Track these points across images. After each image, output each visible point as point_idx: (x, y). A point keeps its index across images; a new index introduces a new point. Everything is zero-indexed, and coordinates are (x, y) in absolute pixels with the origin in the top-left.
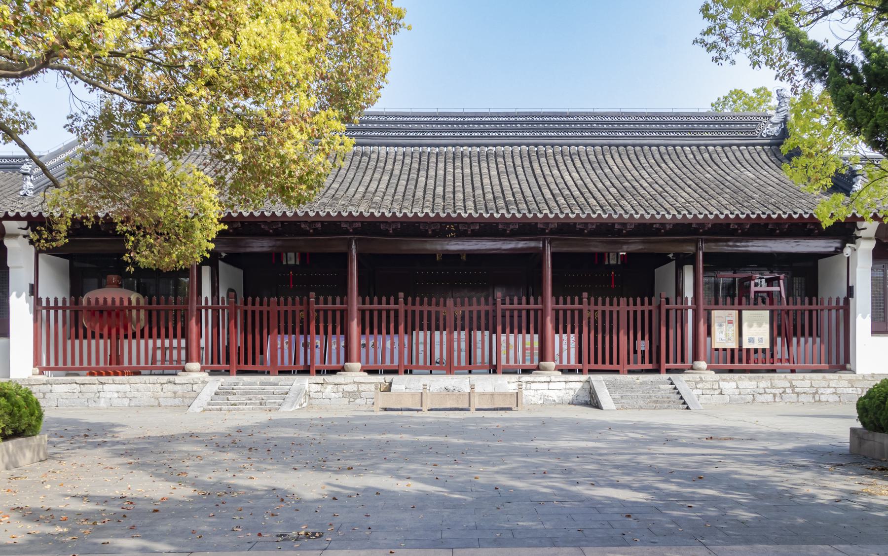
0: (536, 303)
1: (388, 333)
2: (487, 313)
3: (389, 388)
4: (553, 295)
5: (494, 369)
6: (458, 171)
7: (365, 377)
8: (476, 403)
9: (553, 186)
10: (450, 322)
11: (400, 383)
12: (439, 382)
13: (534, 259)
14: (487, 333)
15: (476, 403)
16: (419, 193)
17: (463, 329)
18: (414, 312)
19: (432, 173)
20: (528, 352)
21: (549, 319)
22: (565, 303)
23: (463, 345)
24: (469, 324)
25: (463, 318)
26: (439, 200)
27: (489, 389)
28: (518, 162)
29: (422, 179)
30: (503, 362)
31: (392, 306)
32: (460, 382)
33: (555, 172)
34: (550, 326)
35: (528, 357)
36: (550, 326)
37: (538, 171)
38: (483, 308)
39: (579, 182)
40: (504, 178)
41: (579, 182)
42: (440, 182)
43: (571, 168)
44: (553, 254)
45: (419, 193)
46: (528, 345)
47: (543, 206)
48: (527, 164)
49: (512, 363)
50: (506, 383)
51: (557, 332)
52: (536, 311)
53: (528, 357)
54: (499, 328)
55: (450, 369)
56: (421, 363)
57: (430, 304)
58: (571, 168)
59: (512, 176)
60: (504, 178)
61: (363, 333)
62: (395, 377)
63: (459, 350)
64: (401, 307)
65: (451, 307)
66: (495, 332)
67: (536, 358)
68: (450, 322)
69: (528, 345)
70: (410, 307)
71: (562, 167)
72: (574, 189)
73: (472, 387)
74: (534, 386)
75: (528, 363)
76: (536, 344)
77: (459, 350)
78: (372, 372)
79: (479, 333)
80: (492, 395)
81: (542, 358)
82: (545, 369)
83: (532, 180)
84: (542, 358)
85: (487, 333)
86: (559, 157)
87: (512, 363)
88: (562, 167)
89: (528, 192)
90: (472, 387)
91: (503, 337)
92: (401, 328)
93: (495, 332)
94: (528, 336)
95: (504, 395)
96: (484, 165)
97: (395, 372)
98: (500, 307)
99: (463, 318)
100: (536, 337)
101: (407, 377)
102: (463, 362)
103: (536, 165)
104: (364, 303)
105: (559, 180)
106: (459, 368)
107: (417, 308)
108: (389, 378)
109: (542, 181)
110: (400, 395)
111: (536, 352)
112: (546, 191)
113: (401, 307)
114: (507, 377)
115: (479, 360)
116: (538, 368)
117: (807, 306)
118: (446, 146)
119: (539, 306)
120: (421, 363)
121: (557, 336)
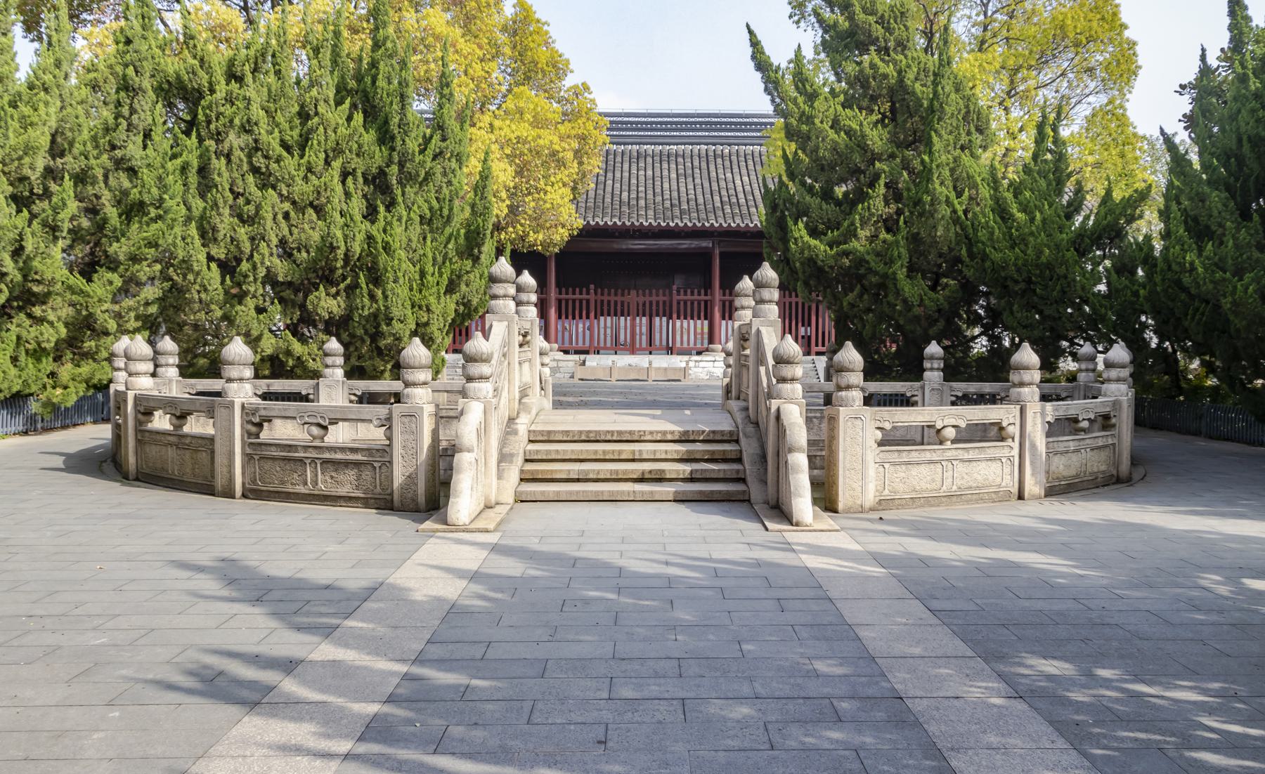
0: (706, 294)
1: (581, 317)
2: (664, 302)
3: (584, 363)
4: (721, 287)
5: (670, 350)
6: (642, 173)
7: (560, 355)
8: (653, 376)
9: (724, 193)
10: (633, 309)
11: (592, 360)
12: (624, 360)
13: (706, 256)
14: (664, 319)
15: (653, 376)
16: (608, 200)
17: (644, 315)
18: (602, 301)
19: (618, 175)
20: (699, 336)
21: (717, 309)
22: (574, 293)
23: (644, 329)
24: (650, 312)
25: (644, 305)
26: (625, 209)
27: (665, 365)
28: (696, 163)
29: (609, 182)
30: (678, 345)
31: (584, 296)
32: (641, 360)
33: (729, 175)
34: (717, 315)
35: (699, 341)
36: (717, 315)
37: (713, 174)
38: (661, 298)
39: (748, 188)
40: (682, 180)
41: (748, 188)
42: (625, 187)
43: (744, 171)
44: (721, 254)
45: (608, 200)
46: (699, 330)
47: (712, 216)
48: (704, 165)
49: (685, 345)
50: (678, 361)
51: (724, 318)
52: (706, 302)
53: (699, 341)
54: (675, 316)
55: (633, 350)
56: (609, 344)
57: (616, 295)
58: (744, 171)
59: (690, 180)
60: (682, 180)
61: (560, 317)
62: (588, 357)
63: (641, 334)
64: (592, 297)
65: (633, 298)
66: (670, 317)
67: (706, 341)
68: (633, 309)
69: (699, 330)
70: (599, 297)
71: (736, 170)
72: (741, 195)
73: (650, 363)
74: (702, 364)
75: (699, 346)
76: (706, 330)
77: (641, 334)
78: (566, 352)
79: (657, 319)
80: (666, 369)
81: (711, 341)
82: (713, 351)
83: (706, 185)
84: (711, 341)
85: (664, 319)
86: (734, 158)
87: (685, 345)
88: (736, 170)
89: (701, 200)
90: (650, 363)
91: (678, 323)
92: (592, 315)
93: (670, 317)
94: (699, 322)
95: (675, 369)
96: (665, 165)
97: (587, 352)
98: (676, 298)
99: (644, 305)
100: (706, 322)
101: (597, 356)
102: (644, 345)
103: (712, 167)
104: (560, 293)
105: (731, 185)
106: (641, 349)
107: (606, 298)
108: (583, 357)
109: (715, 187)
110: (593, 368)
111: (706, 336)
112: (717, 198)
113: (592, 297)
114: (680, 357)
115: (657, 343)
116: (707, 350)
117: (703, 297)
118: (632, 144)
119: (708, 298)
120: (609, 344)
121: (724, 322)
